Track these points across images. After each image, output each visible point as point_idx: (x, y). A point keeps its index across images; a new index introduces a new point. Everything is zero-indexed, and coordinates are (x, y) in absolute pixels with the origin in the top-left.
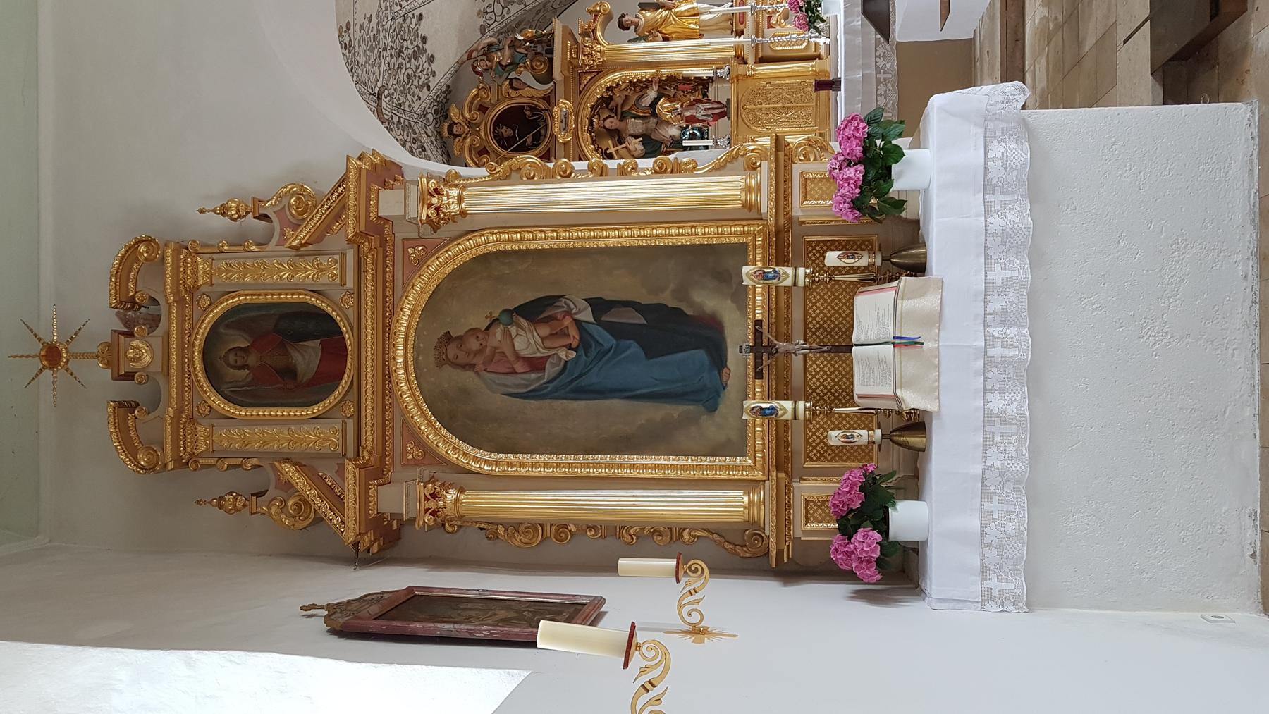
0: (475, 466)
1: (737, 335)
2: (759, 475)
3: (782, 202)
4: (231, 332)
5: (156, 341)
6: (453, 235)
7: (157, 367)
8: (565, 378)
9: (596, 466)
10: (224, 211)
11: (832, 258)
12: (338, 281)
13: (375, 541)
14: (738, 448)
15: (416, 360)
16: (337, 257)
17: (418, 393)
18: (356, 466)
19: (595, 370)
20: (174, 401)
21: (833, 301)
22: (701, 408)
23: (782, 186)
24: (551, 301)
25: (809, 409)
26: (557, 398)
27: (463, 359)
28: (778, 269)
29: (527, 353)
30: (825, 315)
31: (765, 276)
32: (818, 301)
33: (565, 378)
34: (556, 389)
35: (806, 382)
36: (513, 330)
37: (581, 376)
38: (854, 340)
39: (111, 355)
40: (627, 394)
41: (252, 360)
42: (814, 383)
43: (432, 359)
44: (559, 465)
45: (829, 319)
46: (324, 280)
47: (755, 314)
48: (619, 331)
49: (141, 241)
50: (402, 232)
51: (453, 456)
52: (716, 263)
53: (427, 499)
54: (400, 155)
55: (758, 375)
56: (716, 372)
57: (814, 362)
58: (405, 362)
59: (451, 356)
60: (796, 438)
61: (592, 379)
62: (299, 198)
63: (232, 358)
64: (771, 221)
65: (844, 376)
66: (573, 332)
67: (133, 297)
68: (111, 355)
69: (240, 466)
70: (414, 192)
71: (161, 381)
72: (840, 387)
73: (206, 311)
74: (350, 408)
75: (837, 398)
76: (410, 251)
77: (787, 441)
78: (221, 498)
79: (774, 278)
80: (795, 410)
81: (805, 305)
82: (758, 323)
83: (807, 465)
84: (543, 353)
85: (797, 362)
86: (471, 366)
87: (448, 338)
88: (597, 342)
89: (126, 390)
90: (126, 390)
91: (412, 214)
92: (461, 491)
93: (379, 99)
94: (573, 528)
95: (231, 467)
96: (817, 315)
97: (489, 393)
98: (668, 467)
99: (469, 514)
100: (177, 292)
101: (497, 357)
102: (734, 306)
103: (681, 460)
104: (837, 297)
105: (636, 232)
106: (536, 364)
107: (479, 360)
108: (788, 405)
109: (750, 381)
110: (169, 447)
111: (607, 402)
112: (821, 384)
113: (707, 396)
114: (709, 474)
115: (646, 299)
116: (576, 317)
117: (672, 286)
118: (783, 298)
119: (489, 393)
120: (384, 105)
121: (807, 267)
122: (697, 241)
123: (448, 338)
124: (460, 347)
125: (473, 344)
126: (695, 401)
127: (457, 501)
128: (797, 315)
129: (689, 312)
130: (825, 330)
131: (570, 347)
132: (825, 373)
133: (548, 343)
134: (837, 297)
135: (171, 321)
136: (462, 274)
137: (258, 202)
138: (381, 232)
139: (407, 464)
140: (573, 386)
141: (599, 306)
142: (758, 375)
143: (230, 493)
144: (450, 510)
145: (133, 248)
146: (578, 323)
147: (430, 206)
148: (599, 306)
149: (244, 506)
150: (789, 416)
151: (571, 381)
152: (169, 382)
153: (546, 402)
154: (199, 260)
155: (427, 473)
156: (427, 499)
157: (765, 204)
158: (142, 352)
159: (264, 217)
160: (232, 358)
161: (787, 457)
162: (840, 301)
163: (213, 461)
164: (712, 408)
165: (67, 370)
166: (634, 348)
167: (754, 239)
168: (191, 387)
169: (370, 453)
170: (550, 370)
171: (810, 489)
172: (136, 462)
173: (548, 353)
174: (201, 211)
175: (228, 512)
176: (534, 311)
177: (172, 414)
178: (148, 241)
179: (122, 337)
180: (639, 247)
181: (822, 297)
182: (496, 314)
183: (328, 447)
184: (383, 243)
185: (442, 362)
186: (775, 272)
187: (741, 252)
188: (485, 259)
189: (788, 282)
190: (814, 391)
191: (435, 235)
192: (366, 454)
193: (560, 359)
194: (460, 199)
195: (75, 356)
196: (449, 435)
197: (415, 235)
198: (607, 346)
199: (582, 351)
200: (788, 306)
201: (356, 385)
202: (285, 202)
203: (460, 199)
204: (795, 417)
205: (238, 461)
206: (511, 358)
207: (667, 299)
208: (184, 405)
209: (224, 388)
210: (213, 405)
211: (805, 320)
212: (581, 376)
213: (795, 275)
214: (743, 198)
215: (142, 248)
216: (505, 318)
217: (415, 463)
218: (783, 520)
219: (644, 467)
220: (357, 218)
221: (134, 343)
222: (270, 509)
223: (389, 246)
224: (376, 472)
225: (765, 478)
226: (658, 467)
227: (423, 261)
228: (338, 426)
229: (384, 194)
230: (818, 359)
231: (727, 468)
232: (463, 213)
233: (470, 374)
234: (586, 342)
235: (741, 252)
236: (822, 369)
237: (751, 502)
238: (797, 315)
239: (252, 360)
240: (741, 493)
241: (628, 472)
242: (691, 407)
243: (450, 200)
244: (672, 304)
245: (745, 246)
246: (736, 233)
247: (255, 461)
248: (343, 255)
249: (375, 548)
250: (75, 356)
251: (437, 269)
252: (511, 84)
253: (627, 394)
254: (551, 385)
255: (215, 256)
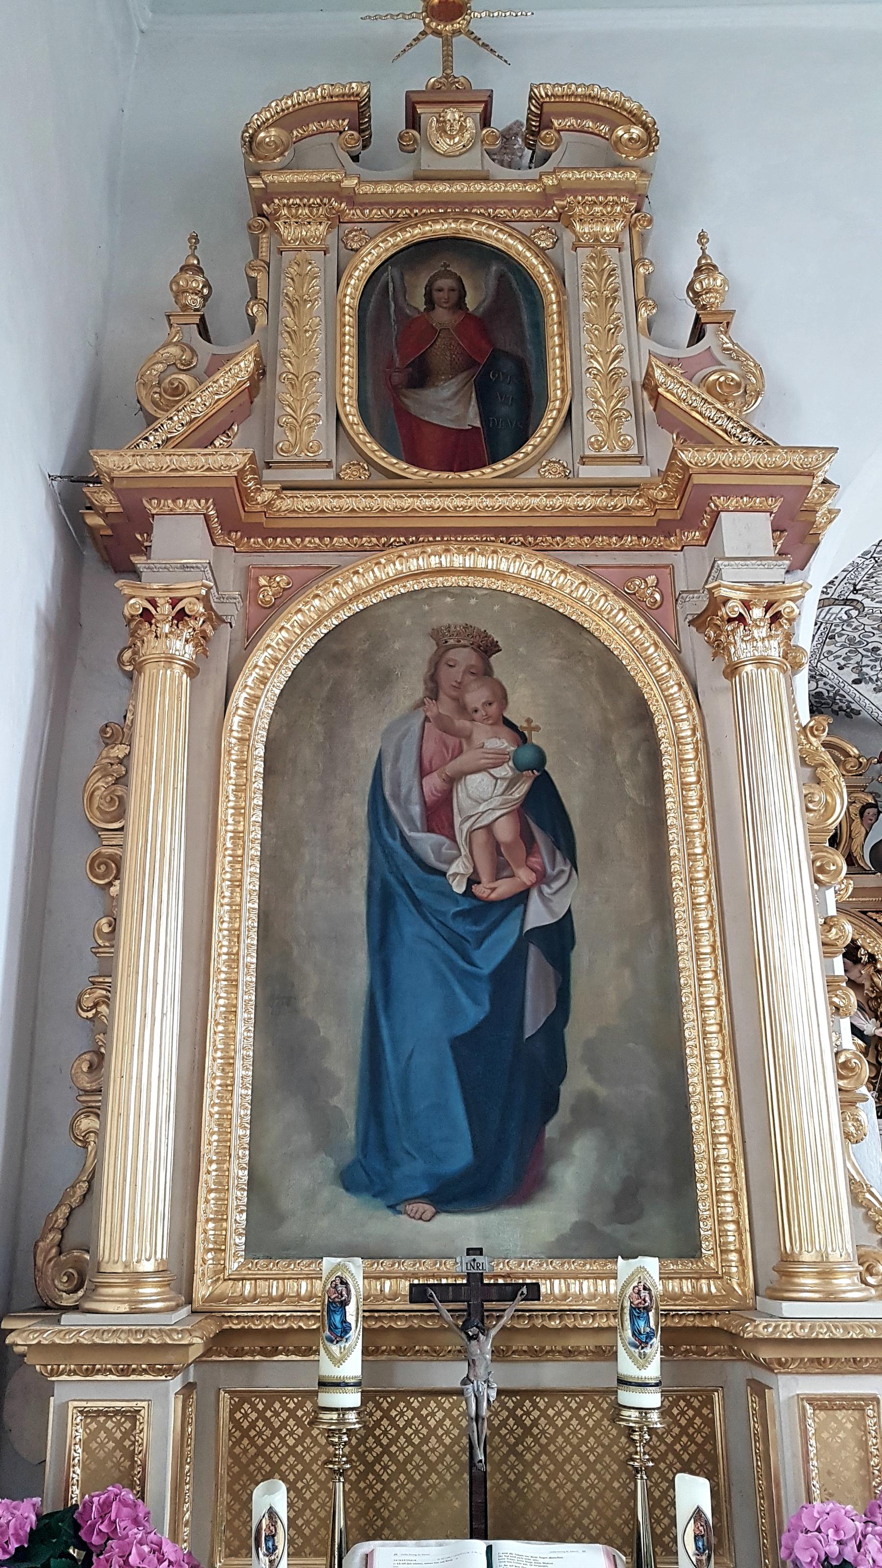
0: (239, 698)
1: (505, 1238)
2: (202, 1291)
3: (808, 1354)
4: (492, 282)
5: (474, 161)
6: (687, 654)
7: (428, 162)
8: (412, 873)
9: (235, 934)
10: (705, 268)
11: (693, 1493)
12: (589, 452)
13: (105, 516)
14: (269, 1237)
15: (445, 591)
16: (634, 451)
17: (383, 595)
18: (242, 471)
19: (429, 933)
20: (368, 189)
21: (584, 1458)
22: (349, 1155)
23: (843, 1354)
24: (564, 841)
25: (341, 1421)
26: (372, 856)
27: (448, 677)
28: (656, 1341)
29: (461, 797)
30: (552, 1440)
31: (639, 1311)
32: (582, 1422)
33: (412, 873)
34: (389, 854)
35: (404, 1394)
36: (506, 771)
37: (416, 902)
38: (505, 1547)
39: (448, 92)
40: (379, 995)
41: (442, 316)
42: (403, 1413)
43: (446, 621)
44: (237, 860)
45: (544, 1449)
46: (590, 429)
47: (550, 1277)
48: (507, 981)
49: (644, 126)
50: (687, 566)
51: (260, 657)
52: (655, 1193)
53: (174, 602)
54: (828, 563)
55: (418, 1293)
56: (424, 1189)
57: (448, 1413)
58: (441, 572)
59: (452, 654)
60: (279, 1373)
61: (410, 926)
62: (738, 385)
63: (445, 283)
64: (762, 1328)
65: (418, 1485)
66: (504, 888)
67: (550, 126)
68: (448, 92)
69: (255, 297)
70: (774, 573)
71: (407, 170)
72: (394, 1476)
73: (529, 241)
74: (350, 475)
75: (370, 1467)
76: (651, 579)
77: (275, 1352)
78: (199, 270)
79: (636, 1333)
80: (339, 1384)
81: (573, 1393)
82: (534, 1292)
83: (224, 1397)
84: (461, 829)
85: (448, 1374)
86: (433, 690)
87: (487, 648)
88: (481, 939)
89: (388, 114)
90: (388, 114)
91: (730, 573)
92: (191, 670)
93: (846, 601)
94: (114, 891)
95: (253, 283)
96: (551, 1421)
97: (382, 726)
98: (228, 1087)
99: (144, 681)
100: (561, 191)
101: (451, 741)
102: (566, 1228)
103: (241, 1111)
104: (591, 1467)
105: (712, 1016)
106: (439, 814)
107: (445, 706)
108: (352, 1367)
109: (408, 1266)
110: (288, 178)
111: (362, 956)
112: (401, 1431)
113: (373, 1174)
114: (208, 1177)
115: (577, 1035)
116: (534, 895)
117: (602, 1092)
118: (587, 1343)
119: (382, 726)
120: (836, 609)
121: (664, 1411)
122: (700, 1147)
123: (487, 648)
124: (469, 671)
125: (476, 696)
126: (364, 1144)
127: (170, 660)
128: (551, 1374)
129: (551, 1130)
130: (520, 1440)
131: (473, 880)
132: (425, 1440)
133: (480, 838)
134: (591, 1467)
135: (510, 183)
136: (611, 672)
137: (725, 320)
138: (687, 522)
139: (249, 577)
140: (397, 888)
141: (558, 939)
142: (418, 1293)
143: (207, 284)
144: (152, 647)
145: (634, 118)
146: (521, 898)
147: (746, 604)
148: (558, 939)
149: (185, 307)
150: (328, 1369)
151: (405, 885)
152: (402, 182)
153: (362, 835)
154: (618, 226)
155: (231, 611)
156: (174, 602)
157: (799, 1313)
158: (453, 137)
159: (698, 334)
160: (445, 283)
161: (241, 1352)
162: (584, 1476)
163: (264, 254)
164: (351, 1180)
165: (424, 33)
166: (473, 1012)
167: (713, 1276)
168: (395, 221)
169: (270, 505)
170: (427, 843)
171: (161, 1411)
172: (265, 125)
173: (461, 839)
174: (702, 237)
175: (175, 281)
176: (543, 809)
177: (346, 183)
178: (650, 140)
179: (480, 108)
180: (680, 1023)
181: (591, 1432)
182: (536, 739)
183: (283, 438)
184: (665, 529)
185: (442, 640)
186: (649, 1336)
187: (684, 1245)
188: (642, 715)
189: (627, 1366)
190: (386, 1414)
191: (683, 624)
192: (267, 495)
193: (450, 862)
194: (762, 662)
195: (447, 43)
196: (301, 652)
197: (681, 586)
198: (477, 955)
199: (465, 905)
200: (569, 1354)
201: (393, 483)
202: (729, 364)
203: (762, 662)
204: (324, 1384)
205: (262, 293)
206: (451, 768)
207: (577, 1082)
208: (363, 206)
209: (392, 272)
210: (364, 251)
211: (541, 1393)
212: (416, 902)
213: (643, 1385)
214: (806, 1257)
215: (636, 131)
216: (527, 755)
217: (250, 590)
218: (91, 1359)
219: (230, 1035)
220: (717, 470)
221: (469, 123)
222: (176, 344)
223: (658, 541)
224: (233, 516)
225: (197, 1304)
226: (229, 1063)
227: (633, 600)
228: (322, 456)
229: (764, 521)
230: (455, 1422)
231: (221, 1217)
232: (732, 670)
233: (419, 691)
234: (485, 913)
235: (684, 1245)
236: (432, 1432)
237: (136, 1279)
238: (551, 1374)
239: (442, 316)
240: (162, 1252)
241: (217, 1002)
242: (351, 1134)
243: (754, 644)
244: (567, 1091)
245: (693, 1252)
246: (724, 1233)
247: (262, 321)
248: (639, 460)
249: (94, 520)
250: (447, 43)
251: (617, 626)
252: (870, 805)
253: (379, 995)
254: (397, 845)
255: (626, 253)
